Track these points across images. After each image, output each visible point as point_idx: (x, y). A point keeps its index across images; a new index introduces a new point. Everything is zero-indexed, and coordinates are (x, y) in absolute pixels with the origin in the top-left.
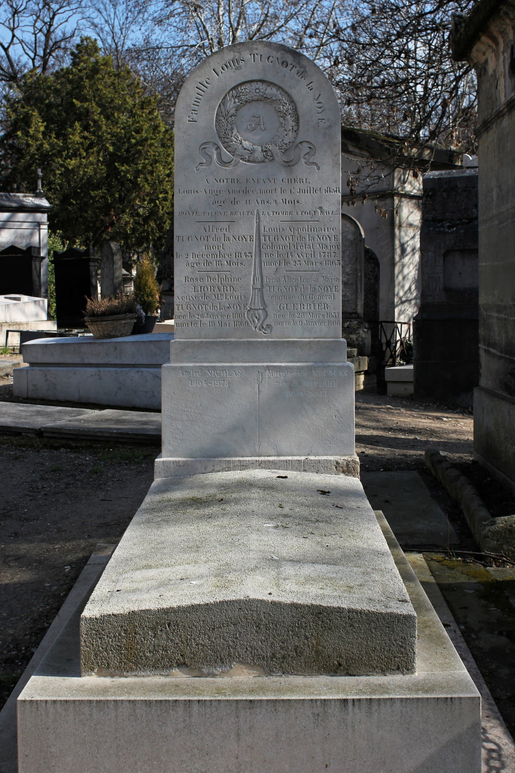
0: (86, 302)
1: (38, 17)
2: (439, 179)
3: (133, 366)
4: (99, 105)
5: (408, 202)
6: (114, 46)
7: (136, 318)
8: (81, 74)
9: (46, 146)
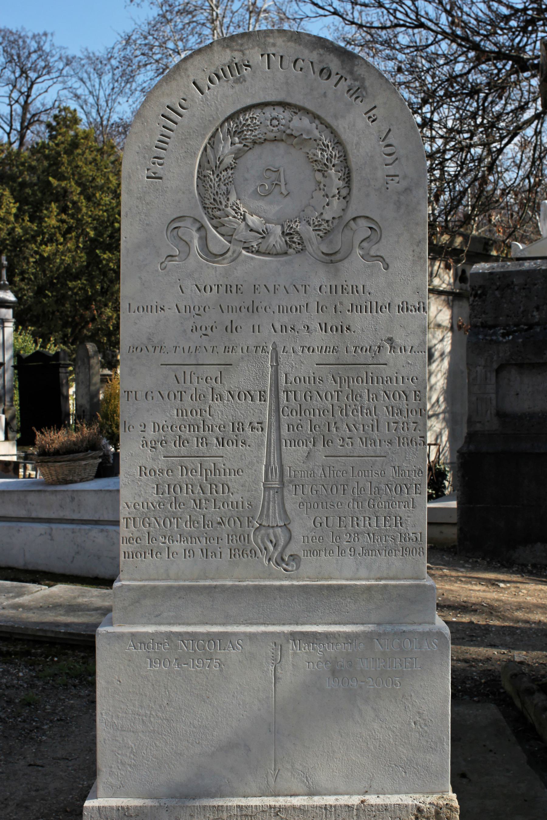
0: (35, 435)
1: (14, 87)
2: (491, 273)
3: (96, 522)
4: (78, 184)
5: (436, 299)
6: (99, 120)
7: (100, 457)
8: (59, 149)
9: (19, 230)
